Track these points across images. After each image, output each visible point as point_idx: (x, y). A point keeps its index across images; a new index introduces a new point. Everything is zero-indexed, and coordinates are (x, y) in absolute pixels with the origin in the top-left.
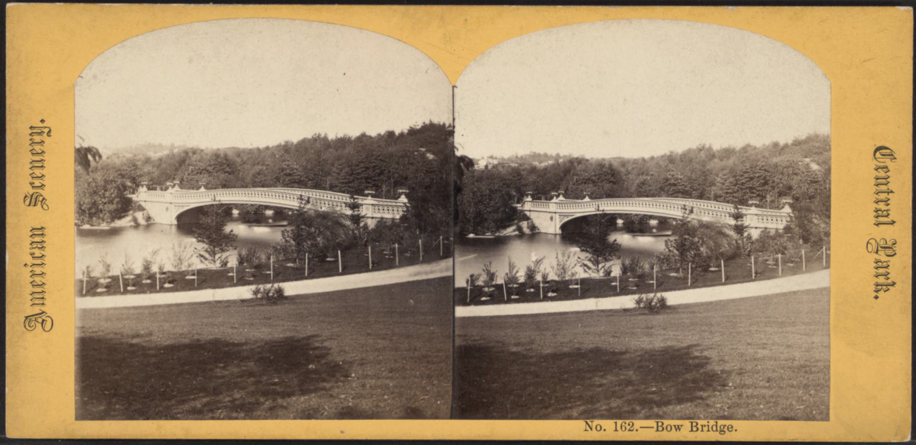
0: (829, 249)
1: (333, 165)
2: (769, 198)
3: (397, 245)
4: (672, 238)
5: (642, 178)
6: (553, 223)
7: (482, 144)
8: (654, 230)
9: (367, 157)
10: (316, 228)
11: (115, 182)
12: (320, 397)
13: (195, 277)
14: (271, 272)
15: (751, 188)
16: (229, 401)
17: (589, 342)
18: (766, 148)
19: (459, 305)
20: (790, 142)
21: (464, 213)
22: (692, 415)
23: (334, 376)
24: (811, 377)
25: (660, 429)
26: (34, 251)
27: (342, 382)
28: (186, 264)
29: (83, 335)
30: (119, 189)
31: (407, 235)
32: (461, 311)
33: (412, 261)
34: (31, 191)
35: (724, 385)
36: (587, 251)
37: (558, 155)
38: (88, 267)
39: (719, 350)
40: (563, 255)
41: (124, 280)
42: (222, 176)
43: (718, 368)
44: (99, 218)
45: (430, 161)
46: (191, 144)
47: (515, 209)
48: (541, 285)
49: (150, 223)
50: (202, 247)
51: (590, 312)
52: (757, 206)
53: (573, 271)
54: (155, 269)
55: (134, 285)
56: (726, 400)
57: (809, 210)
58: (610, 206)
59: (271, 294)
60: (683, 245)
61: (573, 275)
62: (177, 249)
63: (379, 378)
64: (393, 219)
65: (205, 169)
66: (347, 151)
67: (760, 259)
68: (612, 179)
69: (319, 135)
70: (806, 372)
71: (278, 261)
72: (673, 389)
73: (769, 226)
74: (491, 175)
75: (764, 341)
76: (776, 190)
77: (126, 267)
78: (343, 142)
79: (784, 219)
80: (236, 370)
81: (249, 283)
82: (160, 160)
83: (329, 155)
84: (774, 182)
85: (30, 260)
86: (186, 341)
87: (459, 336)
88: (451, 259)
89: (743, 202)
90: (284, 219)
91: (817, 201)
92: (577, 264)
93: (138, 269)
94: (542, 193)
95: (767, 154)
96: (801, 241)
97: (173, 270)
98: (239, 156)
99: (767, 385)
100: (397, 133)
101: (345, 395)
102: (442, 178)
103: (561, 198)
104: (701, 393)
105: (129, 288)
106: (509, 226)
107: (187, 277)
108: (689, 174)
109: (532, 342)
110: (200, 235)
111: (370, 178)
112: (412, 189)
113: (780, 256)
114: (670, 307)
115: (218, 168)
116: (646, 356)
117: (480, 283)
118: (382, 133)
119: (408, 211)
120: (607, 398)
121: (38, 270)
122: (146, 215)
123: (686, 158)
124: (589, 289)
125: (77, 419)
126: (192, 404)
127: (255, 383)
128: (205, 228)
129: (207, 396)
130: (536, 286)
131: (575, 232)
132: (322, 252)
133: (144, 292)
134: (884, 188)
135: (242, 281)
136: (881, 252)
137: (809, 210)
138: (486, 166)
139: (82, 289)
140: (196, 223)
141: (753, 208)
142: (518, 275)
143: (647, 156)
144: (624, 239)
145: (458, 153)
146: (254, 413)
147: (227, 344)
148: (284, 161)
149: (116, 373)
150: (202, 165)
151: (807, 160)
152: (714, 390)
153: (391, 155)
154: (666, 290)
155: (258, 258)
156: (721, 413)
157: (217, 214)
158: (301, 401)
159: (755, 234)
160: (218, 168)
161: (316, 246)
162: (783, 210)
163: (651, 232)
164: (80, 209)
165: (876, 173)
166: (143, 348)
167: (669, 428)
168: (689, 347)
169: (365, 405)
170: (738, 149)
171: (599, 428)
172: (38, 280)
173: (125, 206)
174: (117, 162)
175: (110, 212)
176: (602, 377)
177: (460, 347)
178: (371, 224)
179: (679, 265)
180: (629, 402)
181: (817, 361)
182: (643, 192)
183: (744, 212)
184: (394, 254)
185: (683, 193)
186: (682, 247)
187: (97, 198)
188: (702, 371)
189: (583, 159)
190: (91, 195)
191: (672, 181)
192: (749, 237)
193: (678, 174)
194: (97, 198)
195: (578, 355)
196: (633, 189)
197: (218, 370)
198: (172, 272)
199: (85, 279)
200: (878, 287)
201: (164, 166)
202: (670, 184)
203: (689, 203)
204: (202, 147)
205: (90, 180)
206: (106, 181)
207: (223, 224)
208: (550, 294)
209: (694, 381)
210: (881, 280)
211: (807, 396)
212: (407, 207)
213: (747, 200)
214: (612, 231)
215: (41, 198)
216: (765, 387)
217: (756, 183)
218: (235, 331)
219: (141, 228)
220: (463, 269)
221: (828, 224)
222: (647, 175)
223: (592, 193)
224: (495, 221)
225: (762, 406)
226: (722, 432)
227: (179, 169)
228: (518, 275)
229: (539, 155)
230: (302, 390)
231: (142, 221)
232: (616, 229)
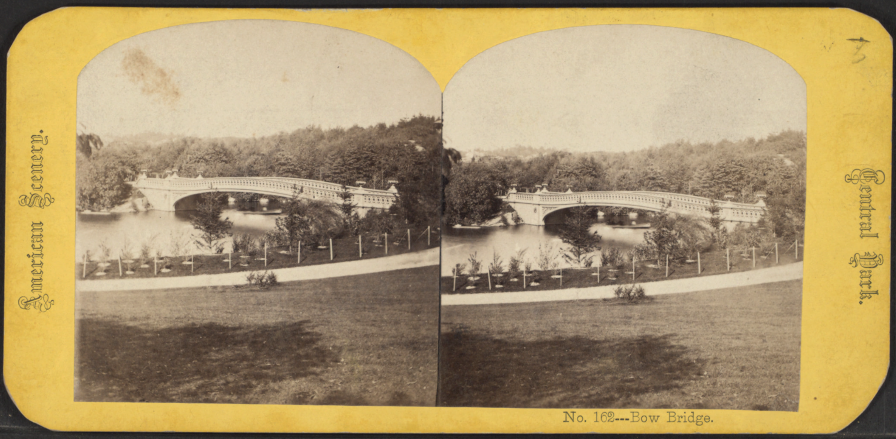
1: (694, 169)
2: (744, 193)
3: (386, 235)
4: (650, 231)
5: (622, 172)
6: (536, 215)
7: (471, 138)
8: (634, 223)
10: (309, 217)
11: (116, 169)
12: (310, 381)
13: (560, 276)
14: (265, 259)
15: (727, 183)
16: (585, 397)
17: (569, 331)
20: (765, 138)
21: (451, 204)
23: (323, 361)
24: (783, 366)
27: (695, 380)
28: (183, 250)
29: (82, 317)
30: (119, 176)
31: (396, 225)
32: (447, 300)
33: (401, 249)
35: (337, 361)
36: (569, 242)
37: (542, 148)
38: (88, 252)
39: (690, 337)
40: (546, 246)
42: (220, 165)
43: (693, 357)
44: (470, 218)
45: (419, 153)
46: (189, 134)
47: (500, 201)
48: (525, 275)
49: (518, 224)
50: (199, 233)
51: (571, 301)
52: (364, 186)
53: (555, 261)
54: (153, 254)
55: (501, 284)
56: (701, 388)
58: (590, 199)
59: (264, 280)
61: (555, 265)
63: (367, 363)
64: (383, 209)
65: (202, 158)
67: (735, 252)
68: (594, 173)
70: (778, 362)
71: (272, 248)
74: (474, 169)
75: (738, 331)
76: (751, 185)
77: (125, 252)
78: (337, 133)
79: (390, 199)
81: (244, 269)
82: (530, 163)
84: (749, 177)
86: (181, 325)
88: (438, 249)
90: (279, 208)
91: (790, 195)
92: (557, 253)
93: (137, 255)
94: (527, 184)
95: (742, 149)
97: (539, 269)
99: (741, 374)
100: (388, 126)
101: (333, 379)
102: (430, 170)
103: (545, 190)
104: (315, 369)
105: (497, 286)
107: (184, 263)
108: (668, 168)
110: (566, 236)
111: (362, 169)
112: (402, 180)
113: (754, 248)
114: (279, 284)
115: (215, 157)
116: (259, 332)
117: (466, 272)
118: (374, 125)
119: (397, 201)
120: (222, 373)
122: (145, 202)
123: (665, 153)
124: (571, 278)
125: (78, 398)
126: (186, 387)
128: (570, 229)
129: (202, 378)
130: (519, 275)
131: (558, 223)
132: (314, 240)
133: (512, 290)
135: (237, 267)
138: (473, 159)
139: (82, 274)
140: (201, 211)
142: (502, 265)
143: (627, 150)
144: (603, 231)
145: (446, 146)
146: (247, 396)
148: (279, 150)
149: (115, 357)
150: (570, 169)
151: (781, 156)
153: (383, 147)
154: (644, 281)
155: (253, 245)
156: (696, 401)
158: (293, 385)
159: (730, 227)
160: (215, 157)
161: (309, 234)
163: (630, 224)
164: (82, 194)
168: (665, 337)
169: (354, 388)
170: (346, 130)
173: (125, 192)
174: (118, 150)
177: (447, 335)
178: (362, 214)
179: (288, 243)
182: (623, 185)
184: (383, 243)
185: (293, 173)
186: (660, 239)
188: (314, 346)
189: (566, 153)
191: (283, 161)
192: (725, 231)
193: (658, 168)
194: (97, 184)
195: (559, 343)
196: (614, 182)
197: (577, 366)
198: (538, 271)
199: (455, 277)
201: (163, 154)
202: (280, 164)
203: (667, 196)
204: (201, 136)
207: (588, 225)
208: (533, 284)
209: (307, 356)
211: (779, 385)
214: (593, 223)
217: (731, 178)
218: (596, 329)
219: (140, 214)
220: (451, 257)
222: (628, 168)
223: (575, 186)
224: (481, 212)
227: (174, 159)
228: (502, 265)
229: (524, 148)
230: (293, 374)
231: (141, 207)
232: (228, 207)
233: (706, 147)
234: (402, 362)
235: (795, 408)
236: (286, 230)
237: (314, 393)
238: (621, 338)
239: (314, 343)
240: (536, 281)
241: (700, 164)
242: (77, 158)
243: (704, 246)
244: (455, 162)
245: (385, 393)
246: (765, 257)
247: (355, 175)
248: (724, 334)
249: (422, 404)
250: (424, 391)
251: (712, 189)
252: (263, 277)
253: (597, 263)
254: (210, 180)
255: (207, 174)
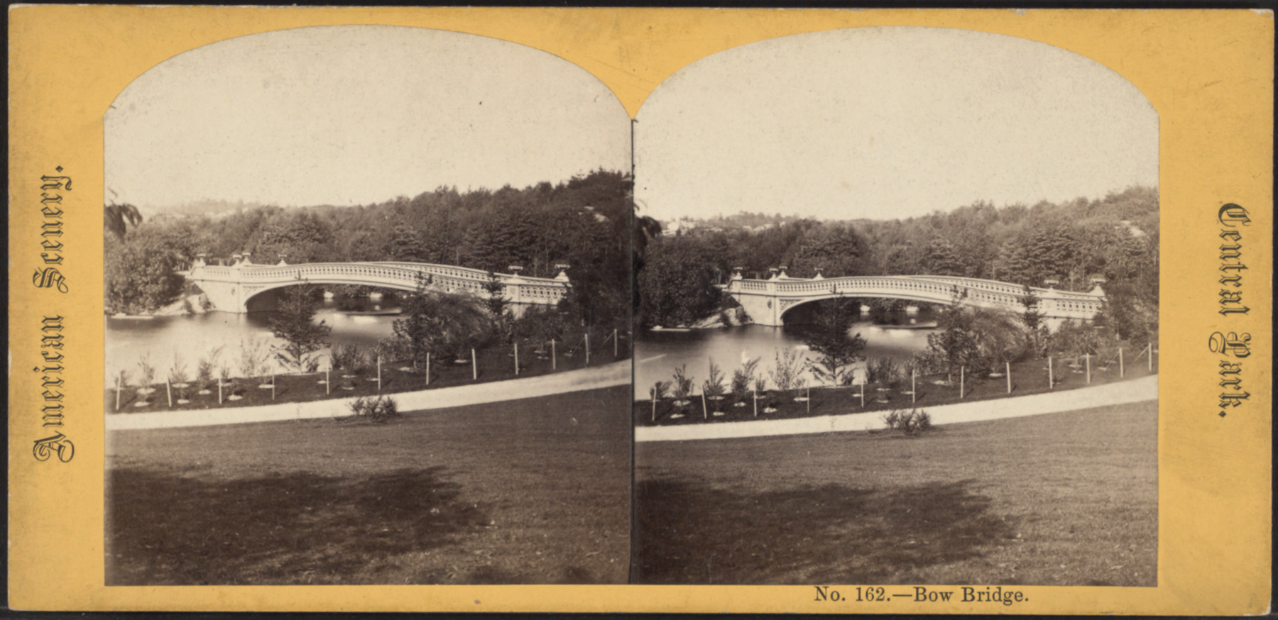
0: (1156, 347)
1: (464, 230)
2: (1072, 276)
3: (553, 342)
4: (937, 332)
5: (896, 248)
6: (772, 311)
7: (673, 201)
8: (913, 321)
9: (512, 219)
11: (161, 253)
12: (446, 553)
14: (379, 379)
15: (1048, 262)
17: (822, 476)
18: (1068, 207)
19: (640, 425)
20: (1102, 198)
22: (966, 579)
23: (465, 524)
24: (1132, 525)
25: (921, 597)
26: (47, 349)
28: (260, 368)
29: (115, 466)
30: (166, 264)
31: (1102, 341)
32: (643, 434)
33: (575, 363)
34: (44, 266)
35: (1010, 537)
37: (778, 215)
38: (122, 372)
39: (1003, 488)
40: (786, 355)
41: (173, 390)
42: (311, 245)
43: (1001, 513)
44: (138, 303)
45: (600, 224)
46: (266, 200)
49: (209, 311)
50: (282, 344)
51: (822, 434)
52: (1056, 287)
53: (800, 377)
54: (216, 374)
55: (187, 398)
56: (1013, 557)
57: (1129, 293)
58: (851, 287)
59: (378, 410)
60: (953, 341)
61: (799, 383)
62: (247, 347)
64: (549, 306)
65: (822, 250)
66: (484, 210)
68: (854, 249)
69: (446, 188)
70: (1125, 518)
71: (388, 363)
72: (939, 542)
73: (1073, 314)
74: (685, 244)
75: (1066, 475)
76: (1083, 265)
77: (176, 372)
79: (1094, 306)
80: (329, 515)
81: (348, 395)
82: (224, 222)
83: (459, 216)
84: (1079, 253)
85: (42, 363)
86: (260, 475)
87: (641, 468)
88: (629, 362)
89: (1037, 282)
90: (397, 305)
91: (1139, 280)
92: (805, 367)
93: (193, 375)
94: (757, 269)
95: (1069, 215)
96: (1118, 336)
97: (241, 375)
98: (333, 217)
99: (545, 522)
100: (554, 185)
101: (481, 550)
102: (616, 248)
103: (783, 275)
104: (979, 548)
105: (181, 402)
106: (710, 315)
107: (261, 386)
108: (961, 243)
109: (742, 477)
110: (278, 328)
111: (517, 248)
112: (575, 263)
113: (1088, 356)
114: (934, 428)
115: (305, 233)
116: (902, 496)
117: (670, 394)
118: (534, 185)
119: (569, 294)
120: (846, 555)
121: (53, 376)
122: (203, 300)
123: (958, 220)
124: (821, 402)
125: (107, 584)
126: (268, 563)
127: (356, 534)
128: (286, 318)
129: (289, 552)
130: (748, 398)
131: (802, 323)
132: (449, 351)
133: (201, 407)
134: (1233, 262)
135: (337, 392)
136: (1230, 352)
137: (1129, 293)
138: (679, 232)
140: (273, 311)
141: (1051, 290)
142: (723, 383)
143: (902, 217)
144: (871, 333)
145: (640, 214)
146: (355, 576)
147: (317, 479)
149: (162, 520)
150: (282, 230)
151: (1127, 223)
152: (997, 543)
153: (546, 217)
154: (929, 404)
155: (895, 373)
156: (1006, 576)
157: (303, 298)
158: (419, 559)
159: (1054, 326)
160: (305, 233)
161: (441, 342)
162: (1092, 293)
163: (908, 323)
165: (1222, 241)
166: (200, 485)
167: (933, 596)
168: (961, 484)
169: (510, 564)
170: (1029, 207)
171: (835, 596)
172: (53, 390)
173: (174, 288)
174: (164, 225)
175: (153, 295)
176: (839, 525)
177: (642, 484)
178: (518, 312)
179: (947, 369)
180: (878, 560)
181: (1140, 503)
182: (897, 267)
183: (1038, 295)
184: (549, 355)
185: (952, 269)
186: (952, 345)
187: (135, 276)
188: (979, 517)
189: (814, 222)
190: (127, 271)
191: (938, 252)
192: (1045, 330)
194: (135, 276)
195: (806, 494)
196: (883, 263)
197: (304, 516)
198: (240, 380)
199: (119, 389)
200: (1225, 401)
201: (229, 231)
202: (935, 257)
203: (962, 282)
204: (282, 205)
205: (126, 251)
206: (148, 253)
207: (311, 312)
208: (767, 410)
209: (969, 531)
210: (1230, 390)
211: (1127, 552)
212: (568, 288)
213: (1042, 279)
215: (57, 277)
216: (1068, 540)
217: (1054, 255)
218: (328, 461)
219: (197, 317)
220: (646, 375)
221: (1155, 312)
222: (903, 243)
224: (691, 308)
225: (1063, 566)
226: (1007, 601)
227: (250, 235)
228: (723, 383)
229: (752, 216)
231: (198, 308)
232: (859, 319)
233: (1015, 213)
234: (580, 524)
235: (1153, 582)
236: (408, 337)
237: (452, 570)
238: (897, 486)
239: (980, 511)
240: (772, 406)
241: (1008, 236)
242: (106, 239)
243: (1017, 354)
244: (653, 236)
245: (555, 568)
246: (1104, 369)
247: (508, 257)
248: (1046, 479)
249: (607, 580)
250: (611, 564)
251: (1026, 271)
252: (376, 405)
253: (860, 378)
254: (297, 268)
255: (293, 259)
